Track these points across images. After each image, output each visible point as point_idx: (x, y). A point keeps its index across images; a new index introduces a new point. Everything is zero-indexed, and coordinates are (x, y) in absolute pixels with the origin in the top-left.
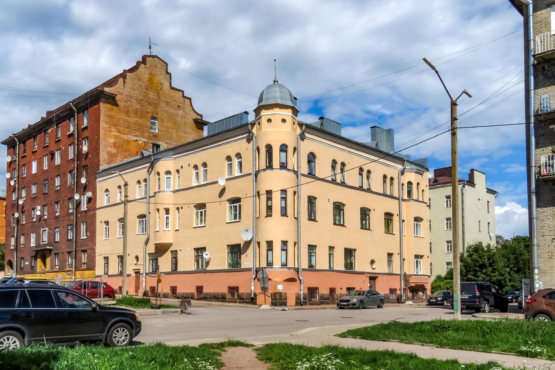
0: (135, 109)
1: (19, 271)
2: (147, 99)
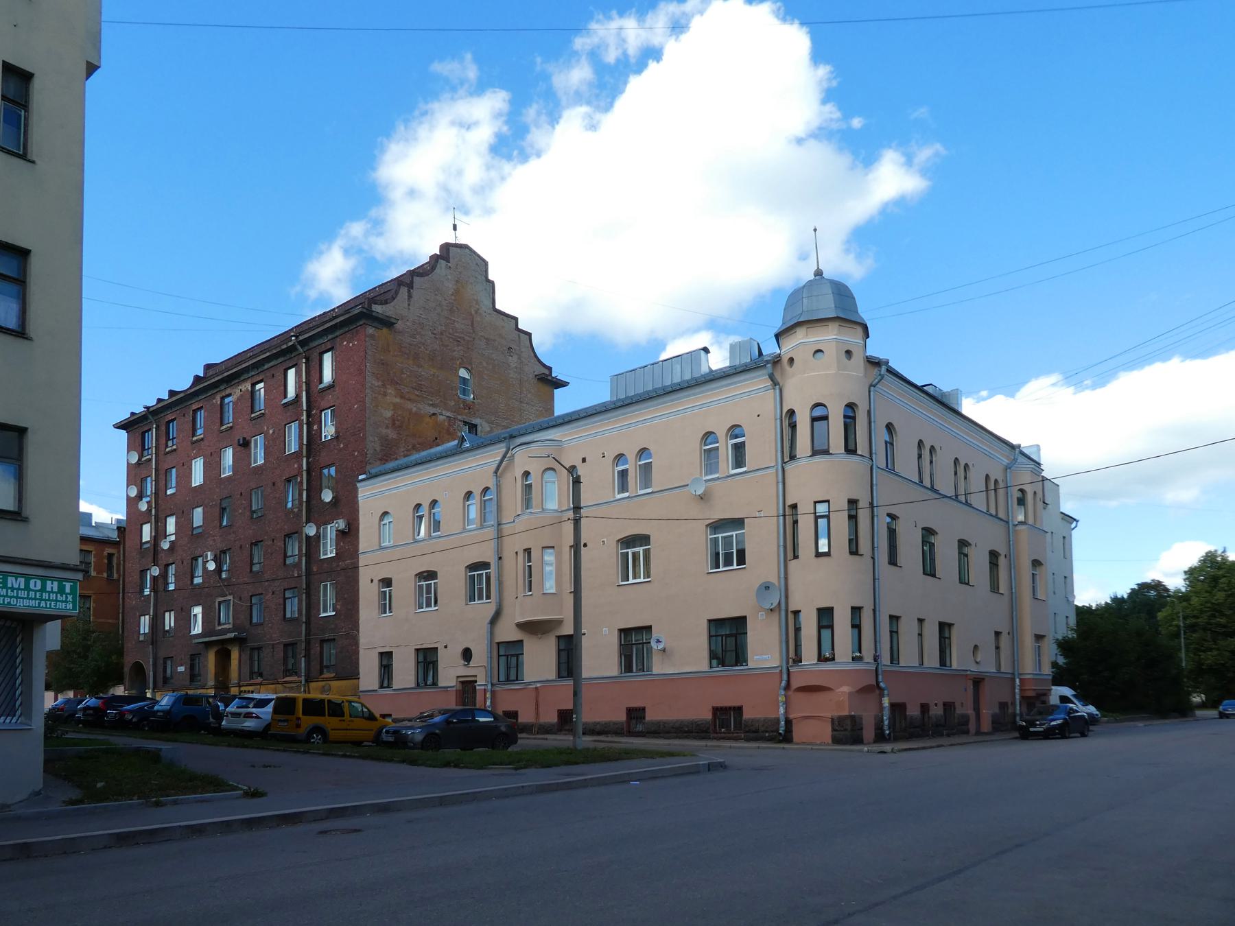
0: (430, 351)
2: (451, 331)
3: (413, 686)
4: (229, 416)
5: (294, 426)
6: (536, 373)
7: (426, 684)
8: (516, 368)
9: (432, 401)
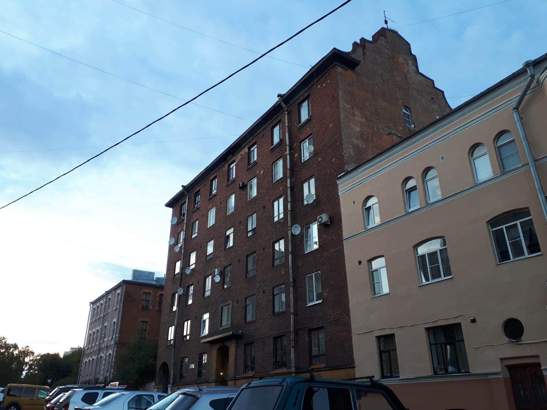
5: (280, 163)
9: (387, 124)
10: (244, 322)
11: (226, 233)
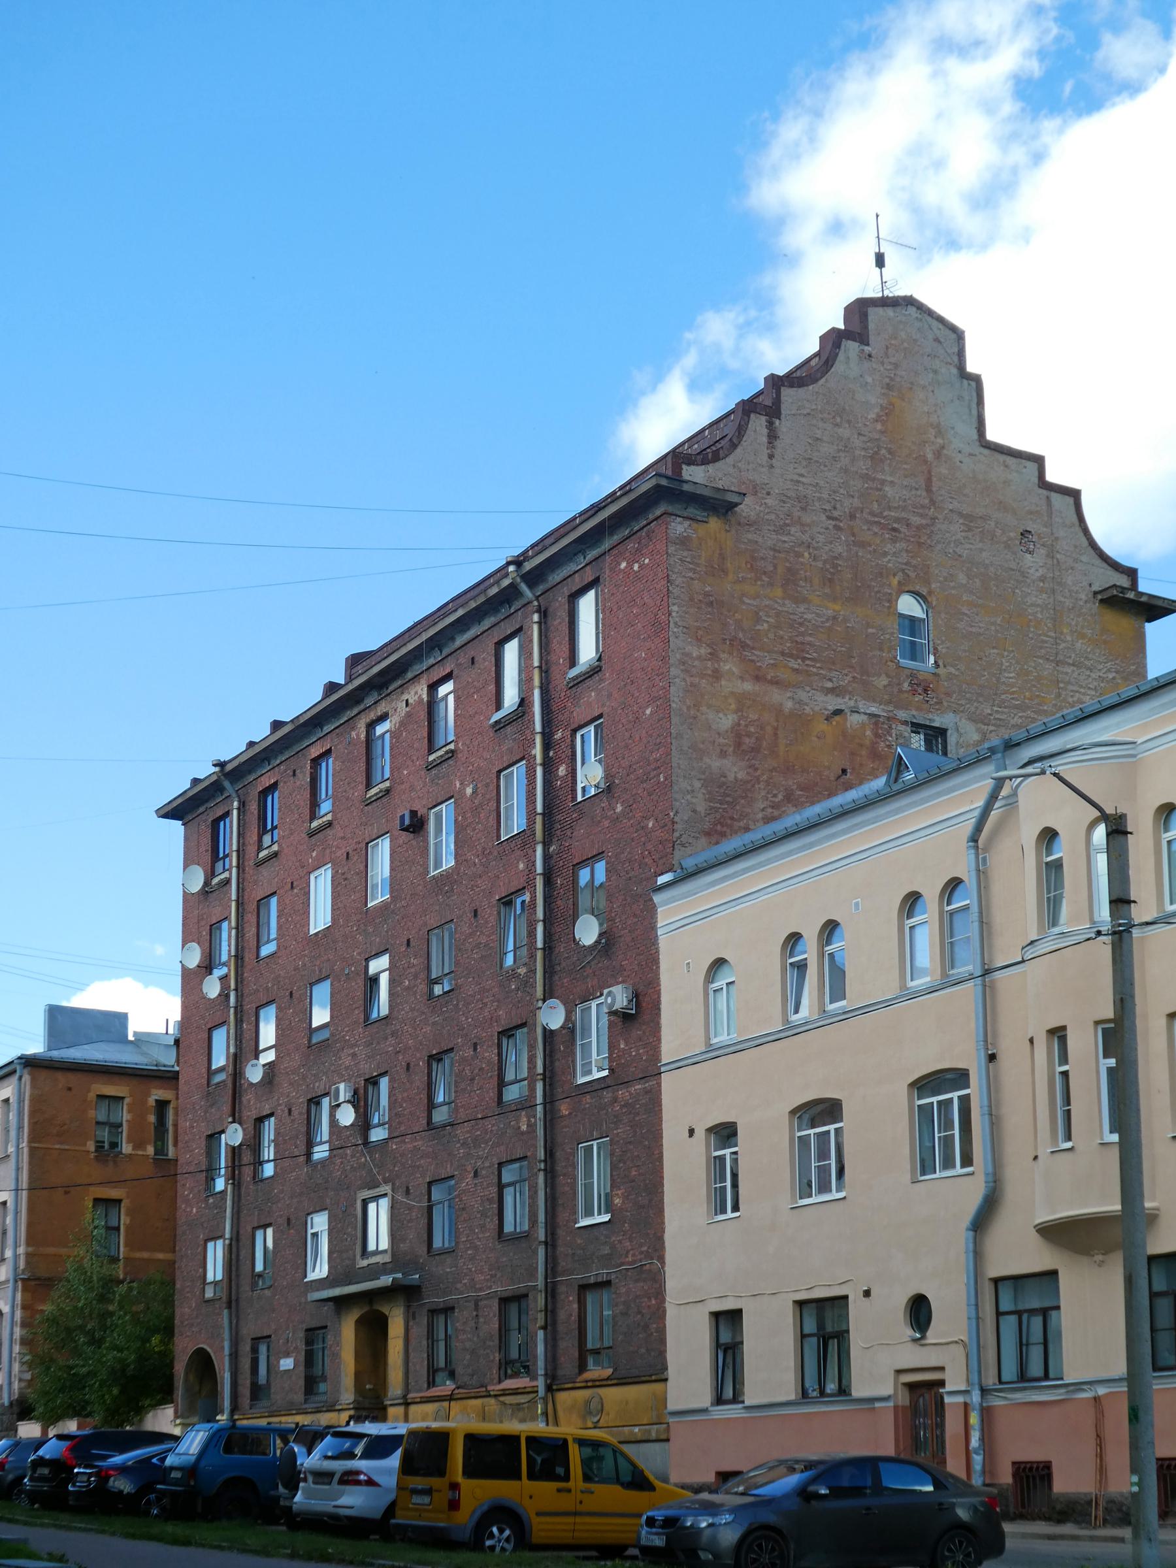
0: (825, 562)
1: (245, 1400)
3: (792, 1397)
4: (384, 765)
6: (1096, 588)
7: (822, 1393)
8: (1043, 579)
9: (830, 680)
10: (426, 1252)
11: (367, 968)
